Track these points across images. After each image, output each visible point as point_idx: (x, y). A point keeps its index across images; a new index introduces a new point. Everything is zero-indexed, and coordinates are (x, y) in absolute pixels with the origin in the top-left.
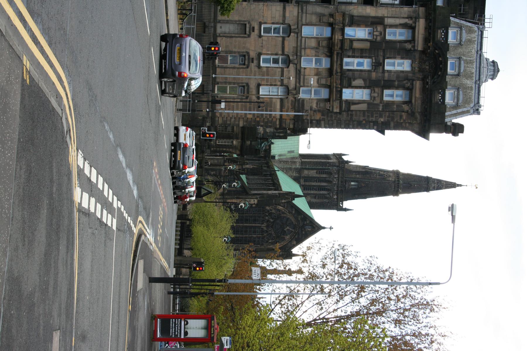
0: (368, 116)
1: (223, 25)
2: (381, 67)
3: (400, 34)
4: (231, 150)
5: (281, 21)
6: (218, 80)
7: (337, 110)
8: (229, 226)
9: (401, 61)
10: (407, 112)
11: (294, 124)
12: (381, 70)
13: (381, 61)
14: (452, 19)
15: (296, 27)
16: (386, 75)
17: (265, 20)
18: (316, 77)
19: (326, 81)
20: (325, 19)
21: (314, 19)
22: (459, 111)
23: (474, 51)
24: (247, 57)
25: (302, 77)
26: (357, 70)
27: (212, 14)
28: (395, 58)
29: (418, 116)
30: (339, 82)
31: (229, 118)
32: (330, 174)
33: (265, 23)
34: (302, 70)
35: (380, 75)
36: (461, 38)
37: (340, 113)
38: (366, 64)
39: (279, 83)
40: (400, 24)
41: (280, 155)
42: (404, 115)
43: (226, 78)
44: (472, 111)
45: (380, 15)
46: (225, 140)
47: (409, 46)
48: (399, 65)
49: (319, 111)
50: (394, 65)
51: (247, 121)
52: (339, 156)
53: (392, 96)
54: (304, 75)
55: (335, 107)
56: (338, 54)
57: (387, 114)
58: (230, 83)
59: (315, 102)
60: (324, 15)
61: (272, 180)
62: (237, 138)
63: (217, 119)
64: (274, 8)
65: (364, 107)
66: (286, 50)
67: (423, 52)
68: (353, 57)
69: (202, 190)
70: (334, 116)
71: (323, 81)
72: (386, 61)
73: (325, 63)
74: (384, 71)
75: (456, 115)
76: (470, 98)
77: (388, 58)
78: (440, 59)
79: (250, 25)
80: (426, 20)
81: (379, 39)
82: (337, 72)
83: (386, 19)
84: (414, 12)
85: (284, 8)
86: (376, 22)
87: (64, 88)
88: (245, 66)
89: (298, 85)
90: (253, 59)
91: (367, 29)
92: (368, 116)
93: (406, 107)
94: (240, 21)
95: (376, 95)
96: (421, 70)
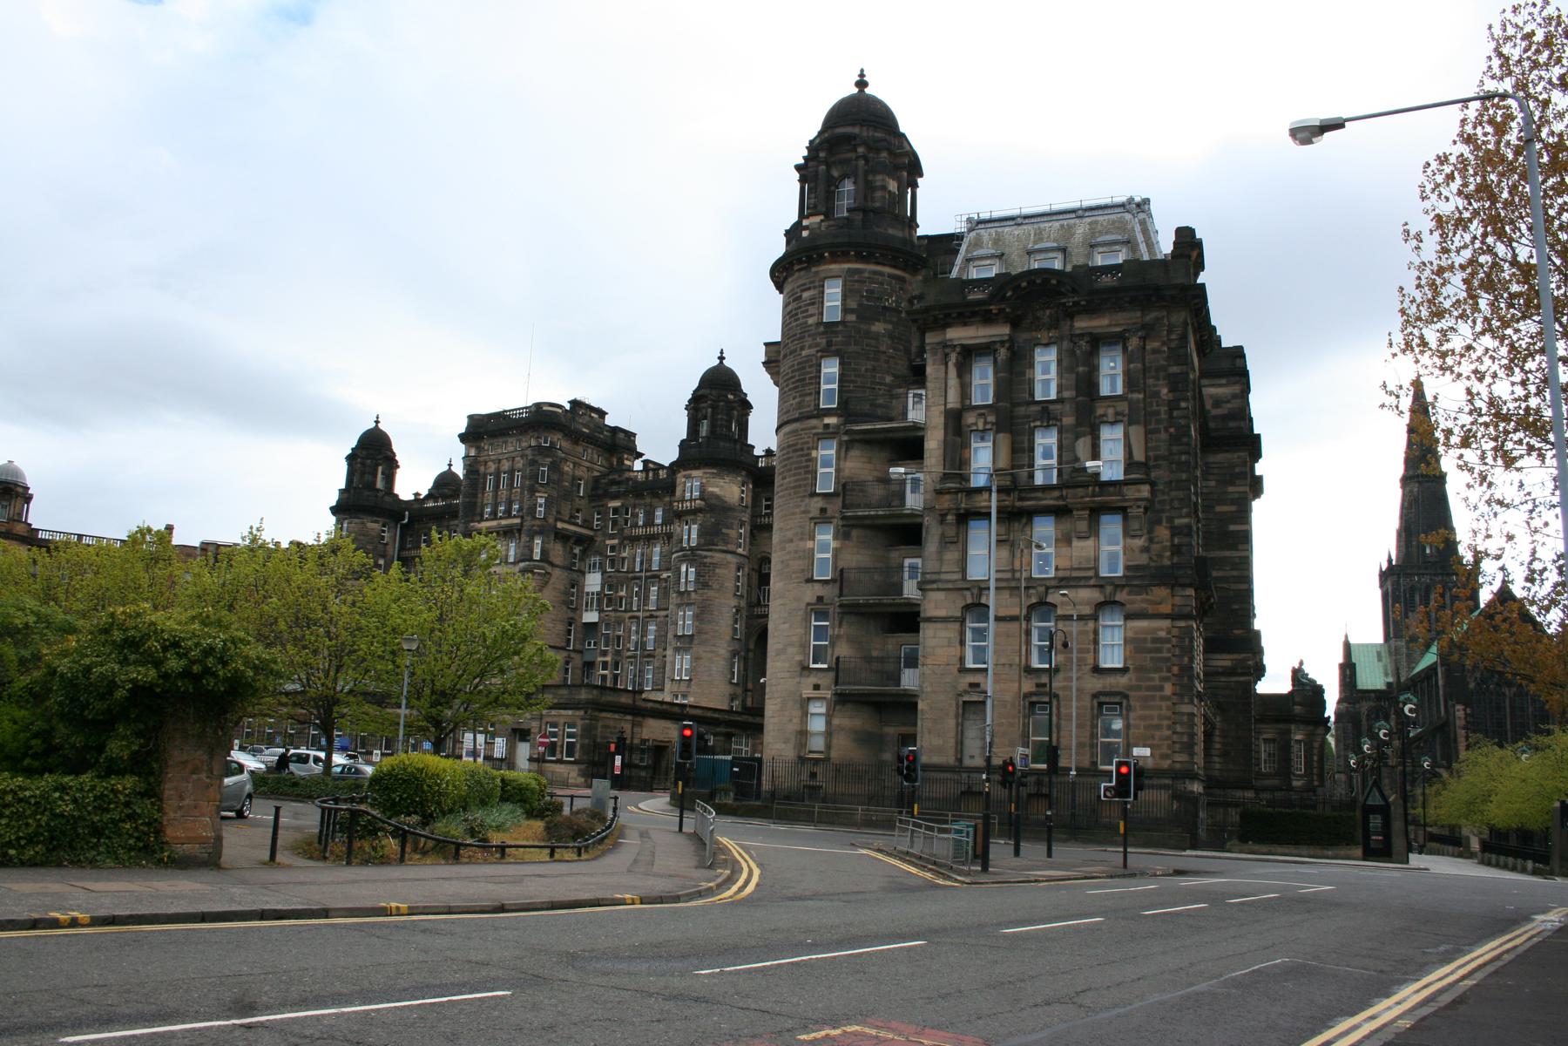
0: (1158, 422)
1: (968, 751)
2: (1051, 407)
3: (984, 377)
4: (1316, 745)
5: (957, 625)
6: (1086, 764)
7: (1145, 491)
8: (1499, 753)
9: (1038, 369)
10: (1144, 339)
11: (1184, 586)
12: (1059, 407)
13: (1038, 408)
14: (954, 274)
15: (968, 593)
16: (1066, 394)
17: (955, 660)
18: (1075, 543)
19: (1080, 519)
20: (951, 532)
21: (952, 555)
22: (1140, 238)
23: (1018, 231)
24: (1034, 699)
25: (1075, 574)
26: (1060, 456)
27: (943, 775)
28: (1031, 382)
29: (1151, 316)
30: (1080, 491)
31: (1175, 738)
32: (1412, 589)
33: (962, 659)
34: (1061, 574)
35: (1067, 407)
36: (987, 258)
37: (1153, 484)
38: (1046, 440)
39: (1091, 625)
40: (960, 376)
41: (1386, 675)
42: (1150, 346)
43: (1080, 745)
44: (1142, 216)
45: (942, 420)
46: (1293, 756)
47: (1003, 353)
48: (1046, 371)
49: (1150, 531)
50: (1046, 383)
51: (1182, 696)
52: (1384, 576)
53: (1113, 377)
54: (1072, 569)
55: (1137, 495)
56: (1021, 499)
57: (1150, 381)
58: (1093, 736)
59: (1129, 541)
60: (943, 536)
61: (1422, 681)
62: (1289, 732)
63: (1178, 766)
64: (930, 643)
65: (1137, 432)
66: (1015, 611)
67: (1015, 324)
68: (1032, 465)
69: (1370, 802)
70: (1160, 497)
71: (1083, 526)
72: (1038, 397)
73: (1044, 528)
74: (1060, 400)
75: (1151, 245)
76: (1114, 222)
77: (1032, 395)
78: (1024, 284)
79: (966, 692)
80: (949, 325)
81: (991, 419)
82: (1061, 497)
83: (949, 406)
84: (934, 353)
85: (929, 620)
86: (956, 423)
87: (1355, 1028)
88: (1055, 703)
89: (1092, 582)
90: (1038, 685)
91: (974, 445)
92: (1158, 422)
93: (1134, 343)
94: (957, 717)
95: (1111, 411)
96: (1054, 325)
